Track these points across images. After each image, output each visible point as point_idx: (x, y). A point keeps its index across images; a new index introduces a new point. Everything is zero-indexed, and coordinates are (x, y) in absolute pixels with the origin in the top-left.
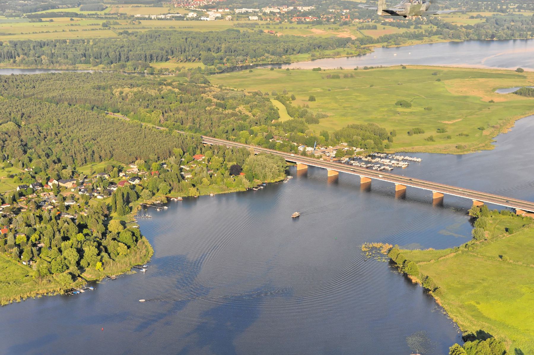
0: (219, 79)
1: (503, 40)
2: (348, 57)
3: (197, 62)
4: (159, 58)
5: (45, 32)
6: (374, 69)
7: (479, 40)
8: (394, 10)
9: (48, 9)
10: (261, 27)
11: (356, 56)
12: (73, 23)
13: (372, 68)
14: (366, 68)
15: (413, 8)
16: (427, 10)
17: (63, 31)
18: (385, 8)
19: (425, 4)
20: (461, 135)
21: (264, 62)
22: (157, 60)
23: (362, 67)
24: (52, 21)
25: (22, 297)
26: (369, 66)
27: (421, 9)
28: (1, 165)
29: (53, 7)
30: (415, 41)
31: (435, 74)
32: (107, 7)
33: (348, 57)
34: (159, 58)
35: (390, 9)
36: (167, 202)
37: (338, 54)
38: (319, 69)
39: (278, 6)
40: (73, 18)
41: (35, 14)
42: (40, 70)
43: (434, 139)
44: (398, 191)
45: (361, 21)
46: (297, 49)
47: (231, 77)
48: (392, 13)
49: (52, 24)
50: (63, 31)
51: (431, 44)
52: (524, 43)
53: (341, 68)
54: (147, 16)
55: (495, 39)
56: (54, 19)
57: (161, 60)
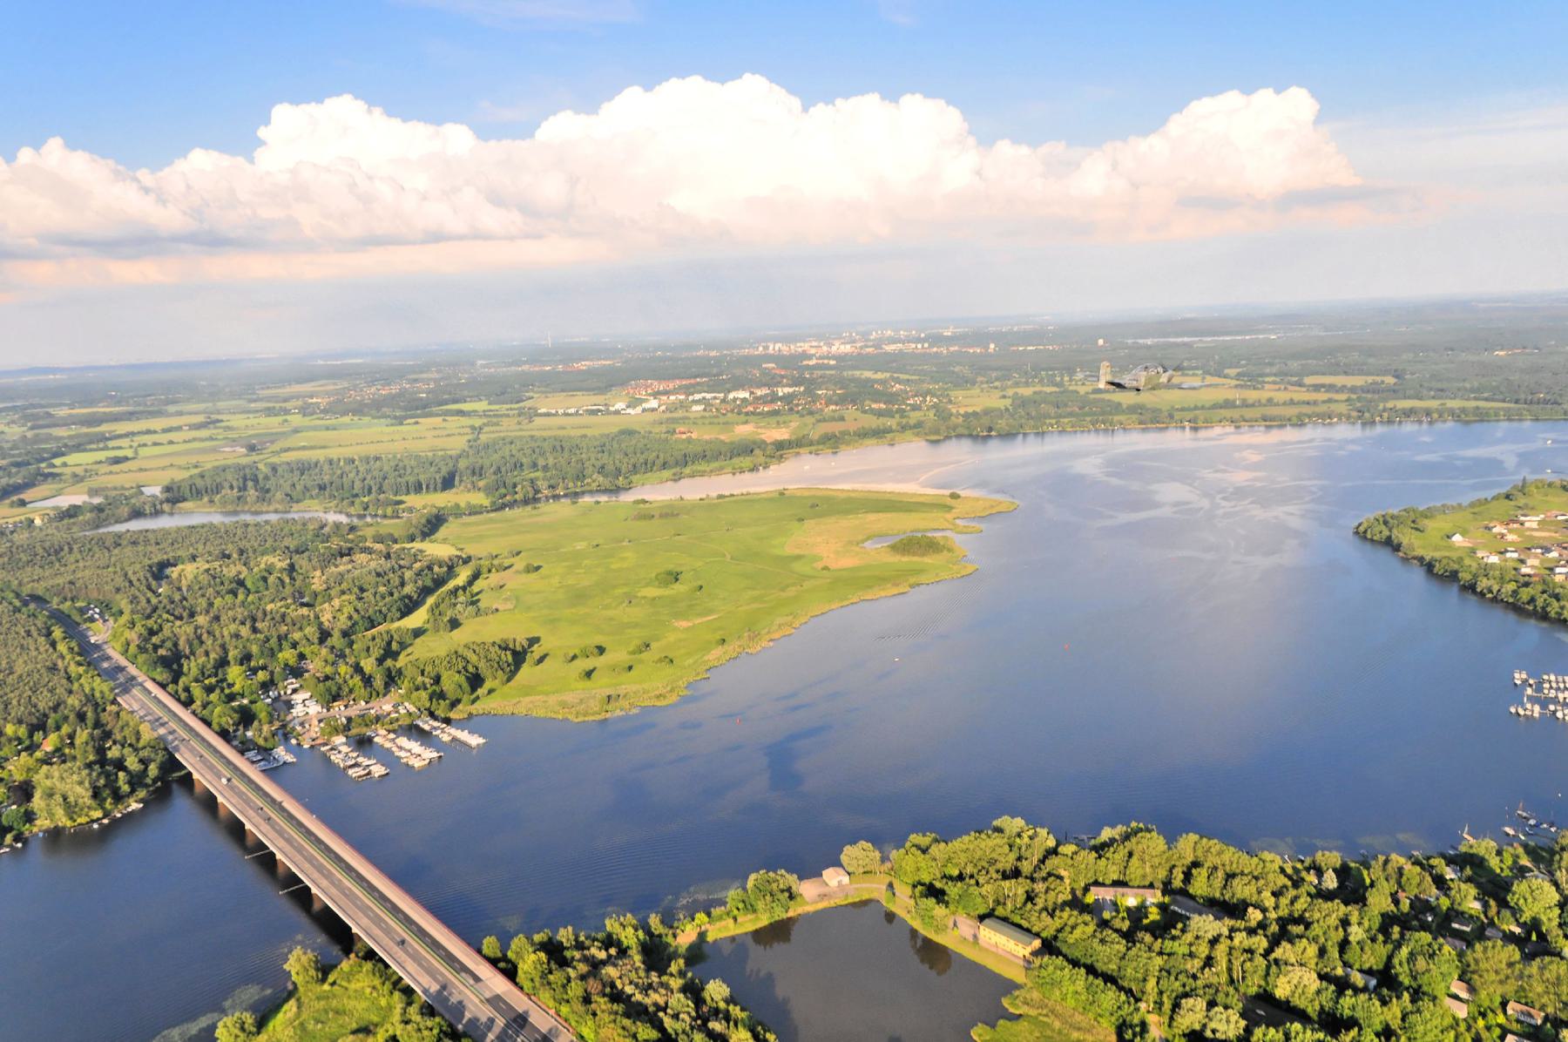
1: (1008, 436)
2: (734, 474)
4: (432, 487)
5: (1209, 409)
6: (727, 499)
7: (970, 436)
8: (1122, 382)
9: (447, 404)
13: (732, 495)
14: (720, 497)
15: (1149, 380)
16: (1169, 381)
17: (404, 439)
18: (1109, 378)
19: (1167, 374)
23: (714, 495)
24: (417, 423)
25: (1425, 523)
26: (727, 493)
27: (1161, 380)
29: (456, 401)
30: (873, 441)
31: (814, 506)
33: (734, 474)
34: (432, 487)
35: (1117, 381)
36: (143, 767)
39: (752, 386)
40: (447, 418)
41: (89, 413)
43: (596, 651)
48: (1119, 386)
50: (404, 439)
51: (892, 445)
52: (1039, 439)
53: (682, 499)
54: (553, 411)
55: (993, 433)
56: (420, 420)
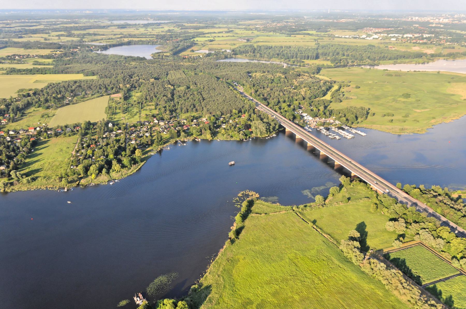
0: (327, 71)
3: (72, 81)
10: (84, 84)
11: (422, 63)
12: (304, 38)
13: (419, 71)
14: (415, 71)
20: (415, 120)
21: (365, 64)
22: (311, 59)
24: (295, 36)
28: (161, 308)
29: (305, 30)
32: (330, 31)
33: (416, 64)
37: (411, 62)
38: (387, 70)
42: (256, 60)
44: (322, 155)
45: (451, 44)
46: (389, 57)
47: (336, 71)
49: (295, 38)
53: (401, 71)
56: (296, 36)
57: (313, 59)
